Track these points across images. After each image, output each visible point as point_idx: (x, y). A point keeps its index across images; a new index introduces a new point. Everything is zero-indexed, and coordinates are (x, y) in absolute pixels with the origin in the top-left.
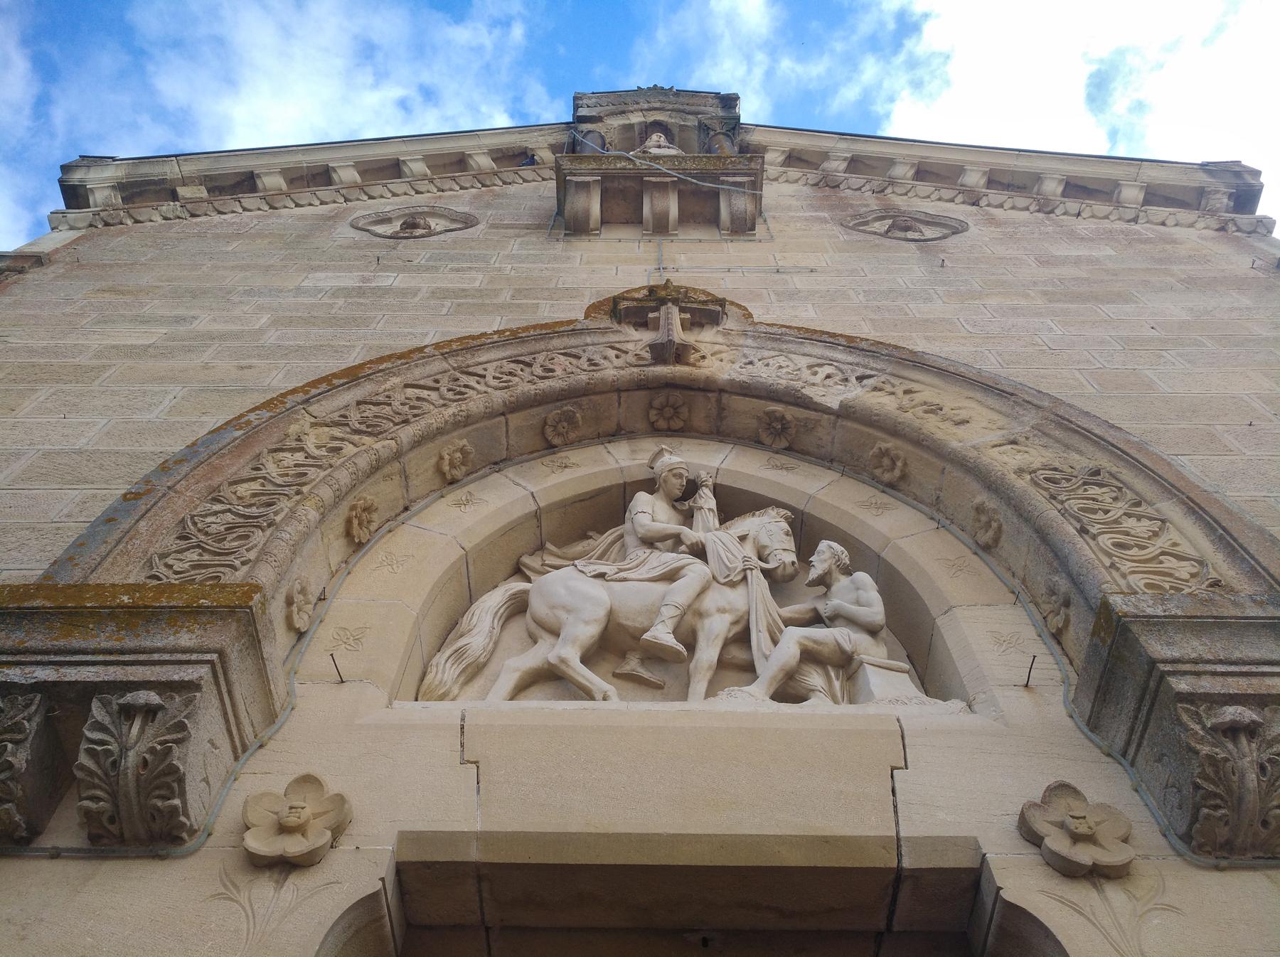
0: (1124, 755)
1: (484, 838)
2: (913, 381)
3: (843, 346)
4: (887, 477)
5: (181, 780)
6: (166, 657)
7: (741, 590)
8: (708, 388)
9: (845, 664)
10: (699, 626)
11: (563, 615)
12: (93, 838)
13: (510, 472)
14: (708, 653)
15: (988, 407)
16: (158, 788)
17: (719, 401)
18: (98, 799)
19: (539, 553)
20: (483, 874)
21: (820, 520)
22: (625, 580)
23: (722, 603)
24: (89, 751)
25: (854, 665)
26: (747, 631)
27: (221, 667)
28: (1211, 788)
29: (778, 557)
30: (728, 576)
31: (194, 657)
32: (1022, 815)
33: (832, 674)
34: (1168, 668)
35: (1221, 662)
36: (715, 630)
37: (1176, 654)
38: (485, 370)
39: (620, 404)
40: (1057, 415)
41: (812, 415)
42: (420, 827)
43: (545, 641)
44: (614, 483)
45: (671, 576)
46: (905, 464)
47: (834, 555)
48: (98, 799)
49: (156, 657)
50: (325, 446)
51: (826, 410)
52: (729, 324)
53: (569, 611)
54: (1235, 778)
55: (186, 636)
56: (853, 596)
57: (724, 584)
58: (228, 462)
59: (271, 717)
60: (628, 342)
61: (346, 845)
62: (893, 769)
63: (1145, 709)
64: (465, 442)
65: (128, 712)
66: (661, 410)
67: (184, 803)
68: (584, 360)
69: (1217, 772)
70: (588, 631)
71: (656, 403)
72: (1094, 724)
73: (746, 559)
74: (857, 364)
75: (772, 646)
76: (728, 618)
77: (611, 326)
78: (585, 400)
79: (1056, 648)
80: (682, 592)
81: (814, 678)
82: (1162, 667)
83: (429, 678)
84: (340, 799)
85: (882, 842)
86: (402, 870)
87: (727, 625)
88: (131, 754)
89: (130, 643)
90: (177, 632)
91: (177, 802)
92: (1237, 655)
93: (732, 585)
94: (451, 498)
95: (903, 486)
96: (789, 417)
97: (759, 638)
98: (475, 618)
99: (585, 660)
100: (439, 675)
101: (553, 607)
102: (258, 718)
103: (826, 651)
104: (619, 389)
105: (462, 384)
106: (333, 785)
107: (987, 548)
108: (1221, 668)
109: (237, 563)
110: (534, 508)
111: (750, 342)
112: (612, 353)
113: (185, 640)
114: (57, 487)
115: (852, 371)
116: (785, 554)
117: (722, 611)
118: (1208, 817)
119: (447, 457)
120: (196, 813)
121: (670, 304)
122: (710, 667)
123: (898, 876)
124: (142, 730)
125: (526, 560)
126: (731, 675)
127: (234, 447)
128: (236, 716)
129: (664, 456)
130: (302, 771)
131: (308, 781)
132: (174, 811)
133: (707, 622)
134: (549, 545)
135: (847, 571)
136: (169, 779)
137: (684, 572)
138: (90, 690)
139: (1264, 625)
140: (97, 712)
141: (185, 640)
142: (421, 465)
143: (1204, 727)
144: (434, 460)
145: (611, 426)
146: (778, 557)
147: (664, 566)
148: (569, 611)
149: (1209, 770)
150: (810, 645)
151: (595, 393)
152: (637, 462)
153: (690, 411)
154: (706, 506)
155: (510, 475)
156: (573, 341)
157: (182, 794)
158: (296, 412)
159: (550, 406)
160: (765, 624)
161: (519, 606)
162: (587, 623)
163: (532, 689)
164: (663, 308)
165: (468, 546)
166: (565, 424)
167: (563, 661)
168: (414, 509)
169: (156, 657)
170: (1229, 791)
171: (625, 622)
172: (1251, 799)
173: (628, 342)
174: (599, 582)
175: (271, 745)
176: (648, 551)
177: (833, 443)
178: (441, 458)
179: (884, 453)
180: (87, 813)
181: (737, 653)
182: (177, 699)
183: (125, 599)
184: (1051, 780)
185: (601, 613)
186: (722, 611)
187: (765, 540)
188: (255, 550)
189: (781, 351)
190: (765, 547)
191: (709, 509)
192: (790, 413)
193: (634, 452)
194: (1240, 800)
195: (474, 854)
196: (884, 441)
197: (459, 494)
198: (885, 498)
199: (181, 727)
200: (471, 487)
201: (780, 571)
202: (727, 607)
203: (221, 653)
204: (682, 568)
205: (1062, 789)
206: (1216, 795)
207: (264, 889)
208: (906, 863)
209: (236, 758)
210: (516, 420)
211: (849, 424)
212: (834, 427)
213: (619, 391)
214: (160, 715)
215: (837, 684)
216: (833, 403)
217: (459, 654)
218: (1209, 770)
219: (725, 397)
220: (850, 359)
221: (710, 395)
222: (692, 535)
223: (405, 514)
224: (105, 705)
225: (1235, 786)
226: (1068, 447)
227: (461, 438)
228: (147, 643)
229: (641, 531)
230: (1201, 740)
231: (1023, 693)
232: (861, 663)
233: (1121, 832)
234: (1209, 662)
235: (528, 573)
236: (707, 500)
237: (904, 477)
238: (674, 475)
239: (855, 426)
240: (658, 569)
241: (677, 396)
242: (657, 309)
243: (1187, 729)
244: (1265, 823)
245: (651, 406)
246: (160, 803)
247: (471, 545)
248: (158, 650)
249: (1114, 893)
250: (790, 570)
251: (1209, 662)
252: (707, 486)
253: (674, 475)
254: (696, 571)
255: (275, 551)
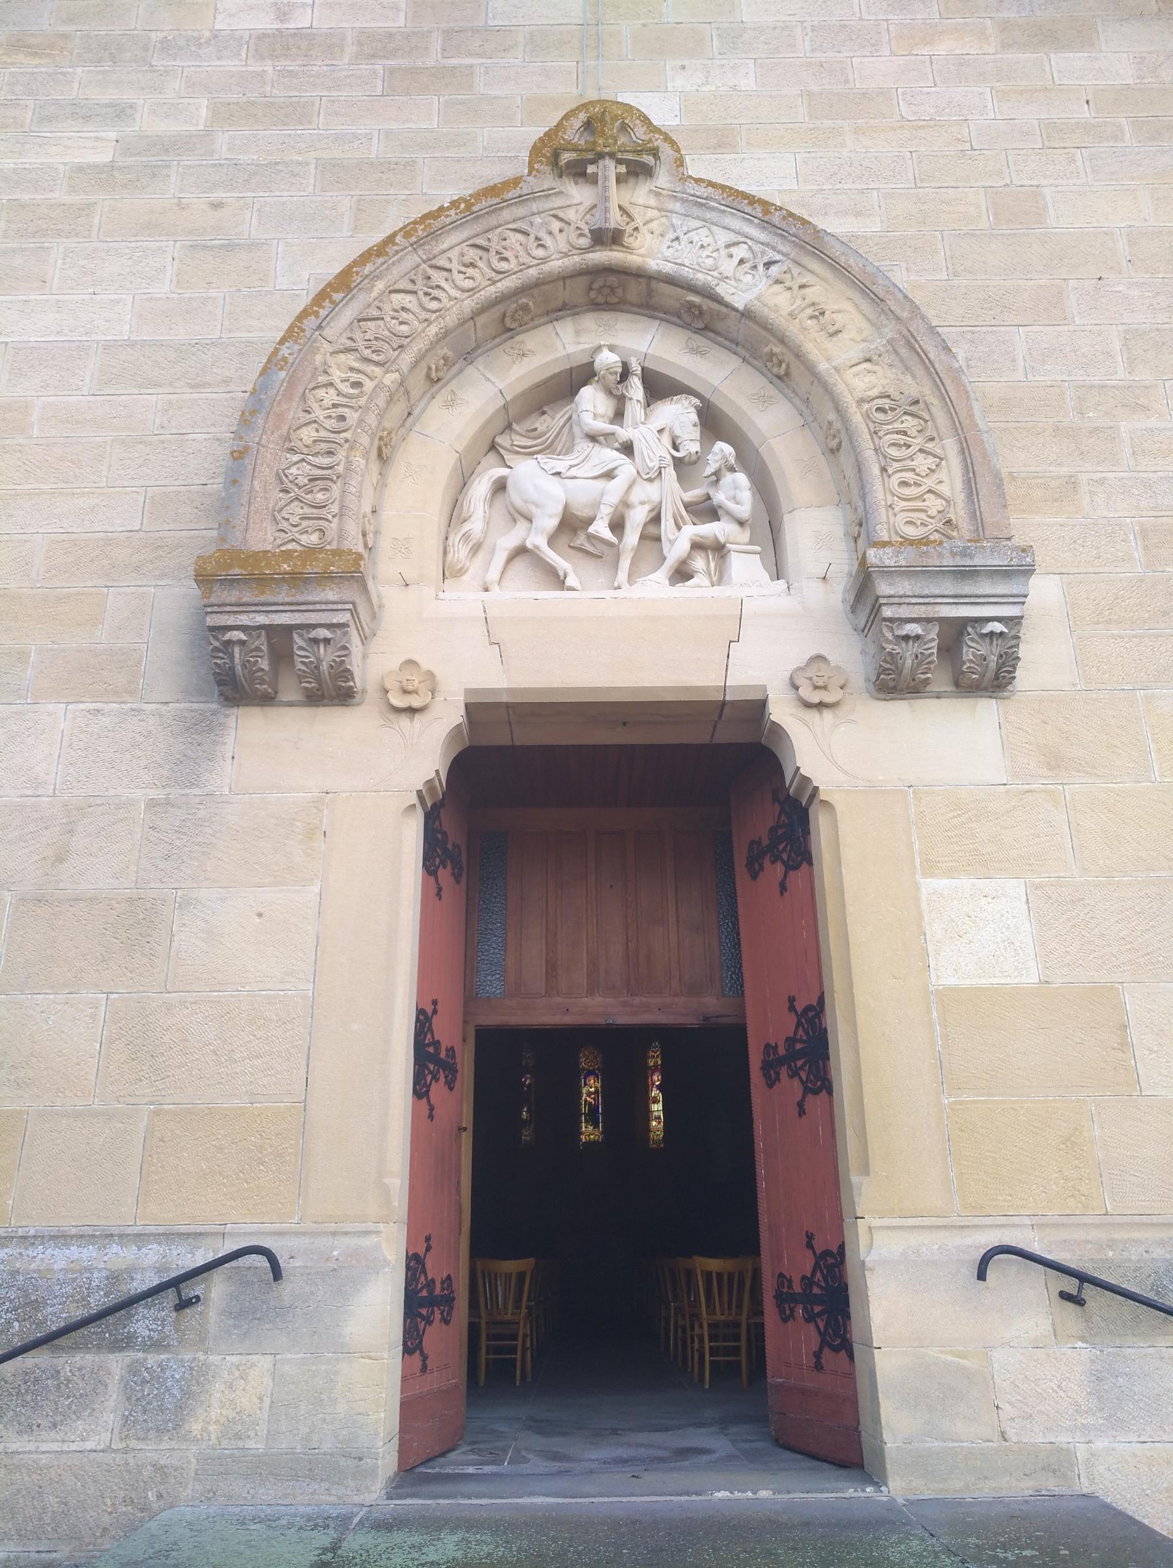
0: (863, 631)
1: (509, 691)
2: (809, 270)
3: (759, 219)
4: (775, 370)
5: (352, 674)
6: (324, 607)
7: (657, 484)
8: (639, 275)
9: (719, 549)
10: (626, 516)
11: (533, 508)
12: (308, 697)
13: (480, 363)
14: (632, 537)
15: (861, 312)
16: (341, 677)
17: (648, 285)
18: (311, 682)
19: (507, 431)
20: (507, 706)
21: (721, 410)
22: (574, 478)
23: (643, 498)
24: (303, 663)
25: (725, 551)
26: (659, 514)
27: (354, 612)
28: (888, 666)
29: (687, 447)
30: (648, 473)
31: (340, 607)
32: (791, 678)
33: (711, 557)
34: (885, 601)
35: (915, 596)
36: (637, 517)
37: (892, 592)
38: (450, 260)
39: (565, 288)
40: (909, 331)
41: (723, 309)
42: (474, 686)
43: (522, 525)
44: (562, 369)
45: (609, 475)
46: (788, 367)
47: (724, 457)
48: (311, 682)
49: (318, 607)
50: (348, 380)
51: (736, 310)
52: (663, 179)
53: (537, 506)
54: (901, 662)
55: (331, 593)
56: (731, 493)
57: (646, 480)
58: (285, 407)
59: (374, 616)
60: (569, 206)
61: (439, 698)
62: (731, 642)
63: (872, 617)
64: (445, 350)
65: (315, 641)
66: (599, 290)
67: (354, 683)
68: (532, 237)
69: (892, 659)
70: (552, 523)
71: (596, 286)
72: (853, 610)
73: (661, 459)
74: (767, 245)
75: (675, 530)
76: (647, 508)
77: (553, 185)
78: (536, 291)
79: (852, 544)
80: (614, 491)
81: (699, 563)
82: (882, 601)
83: (450, 556)
84: (431, 675)
85: (716, 689)
86: (468, 707)
87: (645, 513)
88: (324, 663)
89: (301, 598)
90: (324, 590)
91: (351, 684)
92: (926, 592)
93: (650, 480)
94: (440, 398)
95: (785, 378)
96: (705, 307)
97: (667, 524)
98: (472, 506)
99: (551, 542)
100: (456, 555)
101: (526, 502)
102: (368, 619)
103: (707, 542)
104: (564, 277)
105: (434, 284)
106: (425, 665)
107: (832, 451)
108: (914, 600)
109: (330, 517)
110: (502, 402)
111: (678, 206)
112: (556, 225)
113: (331, 595)
114: (137, 392)
115: (763, 253)
116: (692, 444)
117: (642, 503)
118: (883, 679)
119: (433, 367)
120: (358, 682)
121: (607, 158)
122: (632, 550)
123: (724, 703)
124: (325, 650)
125: (499, 440)
126: (648, 543)
127: (285, 390)
128: (361, 626)
129: (602, 351)
130: (405, 658)
131: (410, 663)
132: (351, 687)
133: (632, 512)
134: (515, 426)
135: (732, 469)
136: (345, 674)
137: (616, 472)
138: (289, 629)
139: (949, 571)
140: (298, 640)
141: (331, 595)
142: (417, 382)
143: (893, 635)
144: (425, 370)
145: (559, 303)
146: (687, 447)
147: (602, 466)
148: (537, 506)
149: (888, 659)
150: (698, 539)
151: (543, 284)
152: (582, 347)
153: (624, 291)
154: (635, 398)
155: (481, 368)
156: (521, 211)
157: (353, 679)
158: (315, 341)
159: (508, 302)
160: (671, 512)
161: (500, 487)
162: (550, 516)
163: (516, 559)
164: (601, 162)
165: (460, 449)
166: (521, 313)
167: (537, 547)
168: (416, 413)
169: (318, 607)
170: (897, 668)
171: (576, 513)
172: (906, 671)
173: (569, 206)
174: (556, 479)
175: (379, 634)
176: (591, 445)
177: (738, 332)
178: (430, 368)
179: (772, 355)
180: (306, 688)
181: (652, 530)
182: (339, 632)
183: (285, 567)
184: (813, 653)
185: (559, 509)
186: (642, 503)
187: (678, 432)
188: (336, 502)
189: (704, 220)
190: (678, 437)
191: (638, 401)
192: (706, 304)
193: (578, 333)
194: (901, 671)
195: (505, 699)
196: (775, 345)
197: (443, 395)
198: (771, 390)
199: (345, 648)
200: (453, 385)
201: (686, 459)
202: (646, 500)
203: (353, 603)
204: (615, 468)
205: (820, 658)
206: (890, 669)
207: (404, 721)
208: (728, 698)
209: (363, 644)
210: (481, 320)
211: (751, 324)
212: (740, 322)
213: (564, 278)
214: (332, 642)
215: (712, 565)
216: (739, 302)
217: (466, 537)
218: (888, 659)
219: (654, 284)
220: (762, 236)
221: (641, 280)
222: (624, 433)
223: (410, 419)
224: (301, 636)
225: (900, 666)
226: (907, 368)
227: (442, 348)
228: (310, 598)
229: (586, 429)
230: (890, 642)
231: (820, 584)
232: (729, 551)
233: (842, 682)
234: (909, 596)
235: (502, 451)
236: (636, 390)
237: (787, 374)
238: (611, 373)
239: (756, 327)
240: (599, 467)
241: (613, 279)
242: (593, 162)
243: (883, 636)
244: (914, 680)
245: (590, 289)
246: (343, 684)
247: (462, 448)
248: (314, 603)
249: (828, 715)
250: (694, 458)
251: (909, 596)
252: (636, 375)
253: (611, 373)
254: (626, 469)
255: (351, 506)
